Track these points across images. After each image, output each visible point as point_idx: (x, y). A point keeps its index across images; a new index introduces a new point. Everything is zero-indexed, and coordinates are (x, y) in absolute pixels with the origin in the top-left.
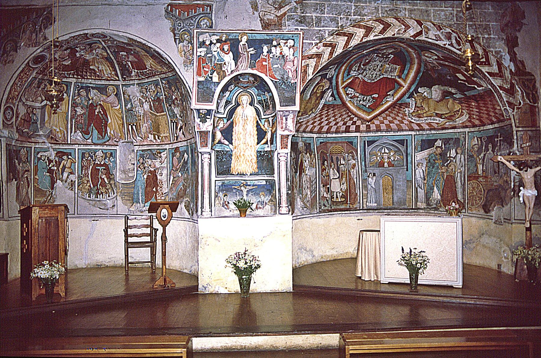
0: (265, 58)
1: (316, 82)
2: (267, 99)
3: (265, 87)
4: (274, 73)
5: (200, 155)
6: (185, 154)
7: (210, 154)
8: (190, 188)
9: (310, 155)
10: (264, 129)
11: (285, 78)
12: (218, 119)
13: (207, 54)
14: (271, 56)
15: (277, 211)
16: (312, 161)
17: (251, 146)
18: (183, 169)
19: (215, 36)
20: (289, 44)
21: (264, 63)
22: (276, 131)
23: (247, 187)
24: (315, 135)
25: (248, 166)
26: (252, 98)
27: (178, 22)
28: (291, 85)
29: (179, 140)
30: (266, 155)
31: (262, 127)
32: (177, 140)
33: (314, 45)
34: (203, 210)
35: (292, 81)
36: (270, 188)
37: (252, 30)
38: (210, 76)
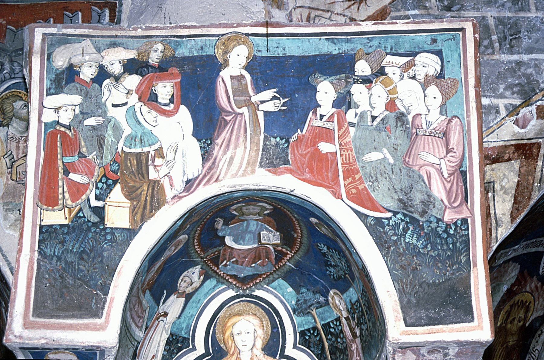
0: (328, 125)
2: (338, 319)
3: (327, 264)
13: (85, 114)
14: (351, 116)
19: (120, 49)
21: (325, 147)
26: (274, 326)
28: (445, 231)
33: (503, 113)
35: (449, 216)
38: (94, 203)
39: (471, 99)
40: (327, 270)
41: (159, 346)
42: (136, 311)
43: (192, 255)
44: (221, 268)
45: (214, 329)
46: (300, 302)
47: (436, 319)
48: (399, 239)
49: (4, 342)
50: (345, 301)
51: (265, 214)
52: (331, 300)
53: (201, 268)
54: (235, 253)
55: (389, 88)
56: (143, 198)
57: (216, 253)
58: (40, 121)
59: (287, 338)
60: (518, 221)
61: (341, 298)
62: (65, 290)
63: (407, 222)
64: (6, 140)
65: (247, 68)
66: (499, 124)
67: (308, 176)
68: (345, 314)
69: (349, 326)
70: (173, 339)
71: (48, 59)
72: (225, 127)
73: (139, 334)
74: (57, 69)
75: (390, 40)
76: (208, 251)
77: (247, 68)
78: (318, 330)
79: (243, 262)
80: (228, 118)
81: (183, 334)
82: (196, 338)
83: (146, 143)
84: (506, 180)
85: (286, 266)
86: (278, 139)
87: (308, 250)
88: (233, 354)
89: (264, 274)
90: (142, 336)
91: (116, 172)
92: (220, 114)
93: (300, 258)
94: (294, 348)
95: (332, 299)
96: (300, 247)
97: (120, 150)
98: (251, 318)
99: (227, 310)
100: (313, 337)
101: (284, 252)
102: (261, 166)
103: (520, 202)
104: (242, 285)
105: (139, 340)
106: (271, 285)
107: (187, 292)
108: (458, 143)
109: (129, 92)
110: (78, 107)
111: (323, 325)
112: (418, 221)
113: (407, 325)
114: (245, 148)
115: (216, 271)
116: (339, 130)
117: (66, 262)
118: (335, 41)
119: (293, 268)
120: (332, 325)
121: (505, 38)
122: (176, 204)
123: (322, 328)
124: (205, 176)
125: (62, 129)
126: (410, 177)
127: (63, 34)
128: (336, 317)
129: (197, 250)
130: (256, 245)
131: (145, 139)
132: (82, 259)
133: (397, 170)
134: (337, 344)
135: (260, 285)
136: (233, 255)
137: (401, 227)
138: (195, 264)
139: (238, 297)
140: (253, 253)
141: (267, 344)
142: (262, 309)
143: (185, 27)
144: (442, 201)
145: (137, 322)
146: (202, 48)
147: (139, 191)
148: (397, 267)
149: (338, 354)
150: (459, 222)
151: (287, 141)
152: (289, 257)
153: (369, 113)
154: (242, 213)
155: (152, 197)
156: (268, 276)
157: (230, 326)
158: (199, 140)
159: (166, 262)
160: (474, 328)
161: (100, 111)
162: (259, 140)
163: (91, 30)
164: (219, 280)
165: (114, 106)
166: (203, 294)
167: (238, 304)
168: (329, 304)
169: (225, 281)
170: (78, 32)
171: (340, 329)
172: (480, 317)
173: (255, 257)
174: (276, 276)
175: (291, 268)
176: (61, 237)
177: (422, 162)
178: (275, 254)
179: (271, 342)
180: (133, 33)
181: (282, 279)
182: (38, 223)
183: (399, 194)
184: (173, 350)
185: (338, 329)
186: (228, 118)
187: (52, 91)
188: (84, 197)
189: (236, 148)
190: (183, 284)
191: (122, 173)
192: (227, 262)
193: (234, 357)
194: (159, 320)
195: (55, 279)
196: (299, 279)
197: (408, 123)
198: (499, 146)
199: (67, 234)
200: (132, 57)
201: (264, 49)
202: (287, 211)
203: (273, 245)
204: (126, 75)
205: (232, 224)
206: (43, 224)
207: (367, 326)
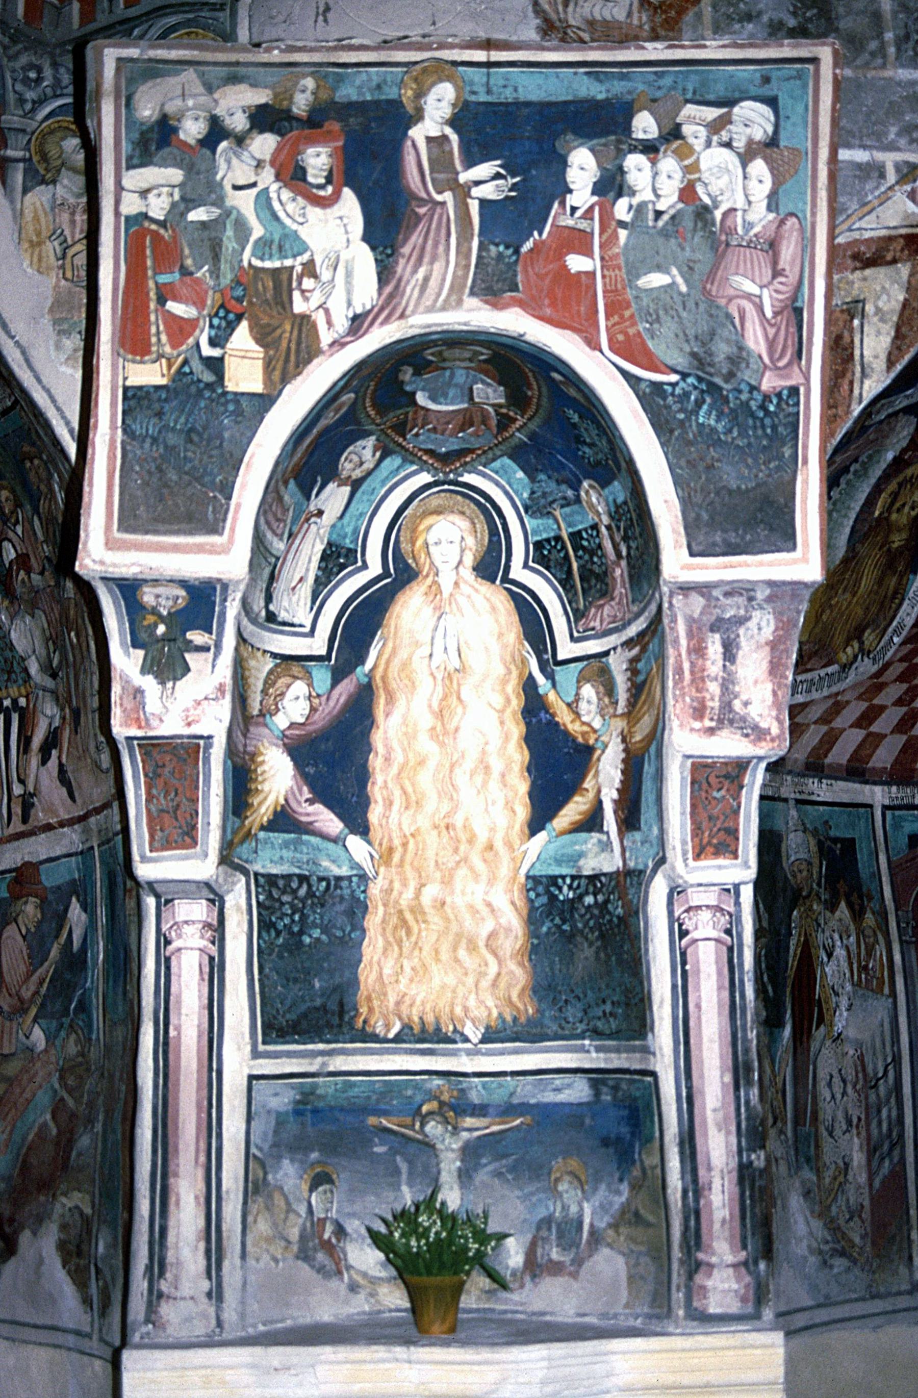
0: (583, 225)
1: (890, 456)
2: (595, 527)
3: (579, 440)
4: (643, 326)
5: (150, 902)
6: (74, 902)
7: (217, 900)
8: (99, 1127)
9: (857, 914)
10: (574, 728)
11: (720, 357)
12: (270, 664)
13: (189, 202)
14: (622, 209)
15: (679, 1296)
16: (870, 952)
17: (490, 847)
18: (58, 1006)
19: (243, 87)
20: (740, 136)
21: (576, 263)
22: (656, 735)
23: (469, 1122)
24: (878, 789)
25: (470, 980)
26: (493, 531)
27: (24, 60)
28: (763, 407)
29: (40, 816)
30: (589, 900)
31: (564, 717)
32: (25, 820)
33: (892, 177)
34: (164, 1286)
35: (768, 383)
36: (625, 1130)
37: (488, 45)
38: (207, 351)
39: (820, 185)
45: (397, 536)
47: (738, 546)
49: (77, 569)
55: (686, 162)
56: (284, 344)
58: (117, 213)
60: (899, 367)
62: (165, 491)
63: (702, 391)
64: (53, 209)
65: (453, 122)
66: (883, 197)
67: (548, 311)
68: (605, 520)
71: (128, 105)
72: (416, 225)
73: (279, 546)
74: (142, 124)
75: (693, 77)
77: (453, 122)
78: (563, 542)
80: (422, 211)
81: (348, 543)
83: (289, 253)
84: (885, 297)
86: (501, 248)
88: (427, 576)
91: (239, 300)
92: (408, 203)
97: (245, 264)
98: (456, 518)
100: (554, 552)
102: (472, 293)
103: (904, 337)
108: (793, 261)
109: (259, 165)
110: (177, 190)
112: (720, 389)
113: (692, 554)
114: (448, 262)
116: (601, 234)
117: (166, 446)
118: (602, 77)
120: (584, 535)
121: (907, 37)
122: (336, 356)
124: (382, 309)
125: (154, 227)
126: (711, 316)
127: (150, 60)
128: (591, 523)
131: (287, 246)
132: (191, 441)
133: (691, 304)
138: (366, 434)
139: (436, 484)
140: (461, 417)
143: (352, 48)
144: (760, 357)
146: (379, 87)
147: (279, 331)
148: (683, 463)
149: (593, 582)
150: (785, 392)
151: (517, 252)
153: (650, 206)
155: (299, 343)
158: (373, 248)
159: (320, 435)
160: (795, 562)
161: (213, 196)
162: (470, 250)
163: (196, 52)
165: (236, 188)
170: (174, 54)
172: (806, 544)
174: (499, 453)
176: (157, 406)
177: (731, 292)
180: (265, 57)
182: (121, 383)
183: (693, 343)
186: (422, 211)
187: (135, 161)
188: (191, 341)
189: (432, 263)
190: (348, 466)
191: (250, 303)
195: (150, 473)
197: (714, 224)
198: (879, 238)
199: (166, 400)
200: (263, 100)
201: (482, 90)
203: (493, 405)
204: (254, 133)
206: (128, 383)
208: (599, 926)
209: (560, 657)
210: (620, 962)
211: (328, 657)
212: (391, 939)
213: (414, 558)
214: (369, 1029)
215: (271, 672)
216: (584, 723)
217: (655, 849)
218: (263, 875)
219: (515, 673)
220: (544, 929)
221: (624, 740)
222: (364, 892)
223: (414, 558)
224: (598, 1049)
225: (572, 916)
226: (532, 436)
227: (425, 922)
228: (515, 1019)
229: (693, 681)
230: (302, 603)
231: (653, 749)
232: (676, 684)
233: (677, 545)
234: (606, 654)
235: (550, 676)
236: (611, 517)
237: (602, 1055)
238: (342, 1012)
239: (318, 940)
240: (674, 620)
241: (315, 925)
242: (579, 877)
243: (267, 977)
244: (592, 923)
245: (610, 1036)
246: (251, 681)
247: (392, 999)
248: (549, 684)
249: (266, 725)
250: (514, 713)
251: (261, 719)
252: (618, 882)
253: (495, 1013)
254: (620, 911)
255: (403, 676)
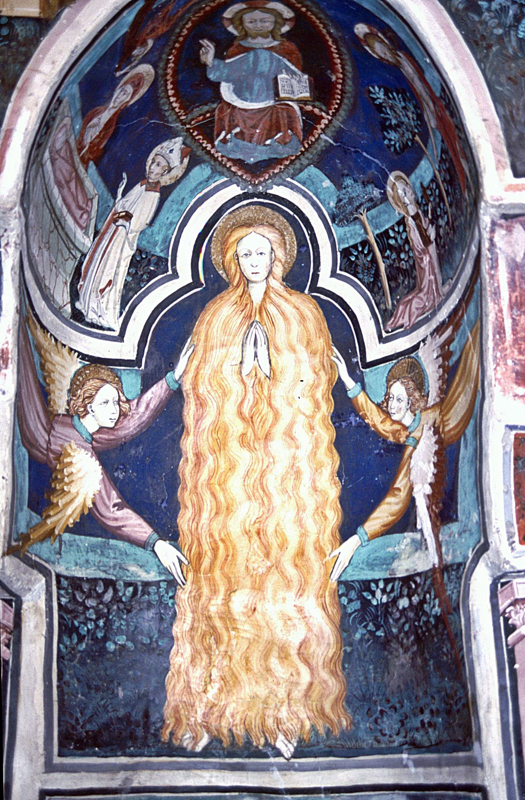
2: (402, 222)
3: (385, 127)
12: (77, 365)
17: (301, 553)
25: (282, 693)
26: (302, 243)
30: (404, 603)
40: (385, 138)
41: (118, 267)
42: (72, 194)
43: (167, 114)
44: (218, 145)
46: (341, 203)
48: (507, 33)
50: (413, 189)
51: (282, 35)
52: (391, 191)
53: (184, 143)
54: (239, 117)
57: (208, 115)
59: (321, 261)
61: (407, 183)
68: (412, 210)
69: (419, 227)
70: (142, 258)
76: (192, 110)
78: (370, 246)
79: (252, 136)
81: (158, 251)
82: (178, 259)
85: (320, 141)
87: (354, 105)
88: (238, 286)
89: (286, 159)
90: (89, 245)
93: (341, 123)
94: (332, 276)
95: (393, 190)
96: (341, 100)
98: (265, 231)
99: (229, 218)
101: (316, 115)
104: (252, 177)
105: (85, 251)
106: (297, 178)
107: (163, 184)
111: (377, 235)
115: (210, 151)
119: (330, 143)
120: (392, 234)
123: (376, 241)
128: (397, 218)
129: (174, 105)
130: (271, 103)
134: (399, 263)
135: (281, 178)
136: (236, 122)
137: (511, 12)
138: (171, 134)
140: (267, 118)
141: (291, 271)
142: (284, 216)
145: (78, 217)
148: (503, 79)
152: (325, 124)
154: (243, 33)
156: (292, 162)
157: (233, 243)
164: (216, 169)
166: (188, 190)
167: (246, 208)
168: (387, 199)
169: (225, 170)
171: (404, 237)
173: (271, 126)
174: (305, 162)
175: (328, 144)
178: (303, 119)
179: (296, 269)
181: (315, 166)
184: (142, 275)
185: (401, 238)
192: (227, 134)
193: (239, 290)
194: (117, 224)
196: (341, 163)
202: (321, 26)
205: (230, 57)
207: (448, 217)
208: (414, 630)
209: (369, 359)
210: (439, 666)
211: (137, 362)
212: (199, 647)
213: (224, 269)
214: (176, 743)
215: (78, 373)
216: (394, 422)
217: (476, 536)
218: (66, 578)
219: (324, 378)
220: (358, 636)
221: (436, 432)
222: (172, 597)
223: (224, 269)
224: (417, 764)
225: (386, 621)
226: (338, 136)
227: (234, 629)
228: (328, 732)
229: (515, 341)
230: (111, 305)
231: (469, 431)
232: (496, 345)
233: (499, 163)
234: (416, 347)
235: (359, 379)
236: (418, 203)
237: (421, 770)
238: (147, 726)
239: (123, 647)
240: (494, 266)
241: (119, 630)
242: (393, 580)
243: (67, 684)
244: (407, 627)
245: (430, 749)
246: (55, 376)
247: (200, 710)
248: (358, 387)
249: (74, 427)
250: (324, 419)
251: (68, 420)
252: (434, 579)
253: (308, 725)
254: (437, 610)
255: (214, 383)
